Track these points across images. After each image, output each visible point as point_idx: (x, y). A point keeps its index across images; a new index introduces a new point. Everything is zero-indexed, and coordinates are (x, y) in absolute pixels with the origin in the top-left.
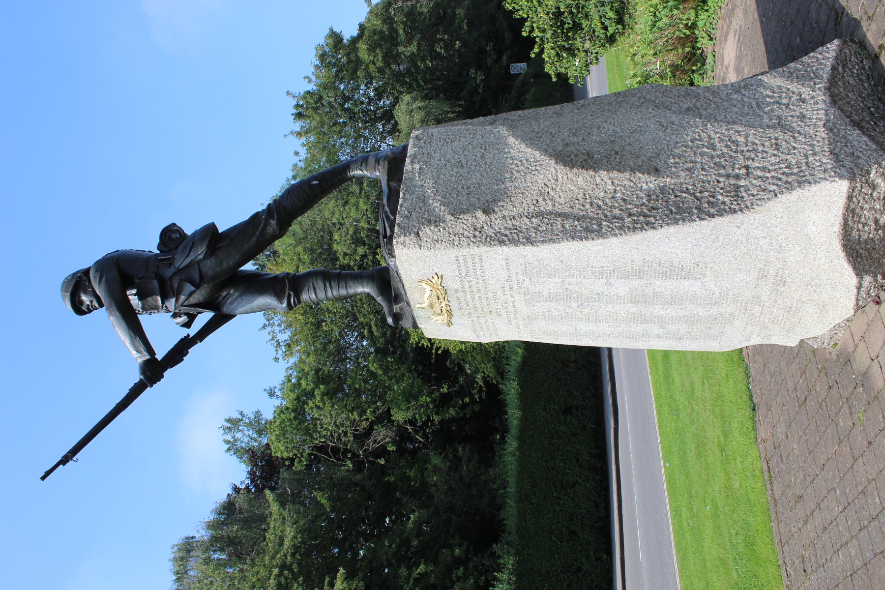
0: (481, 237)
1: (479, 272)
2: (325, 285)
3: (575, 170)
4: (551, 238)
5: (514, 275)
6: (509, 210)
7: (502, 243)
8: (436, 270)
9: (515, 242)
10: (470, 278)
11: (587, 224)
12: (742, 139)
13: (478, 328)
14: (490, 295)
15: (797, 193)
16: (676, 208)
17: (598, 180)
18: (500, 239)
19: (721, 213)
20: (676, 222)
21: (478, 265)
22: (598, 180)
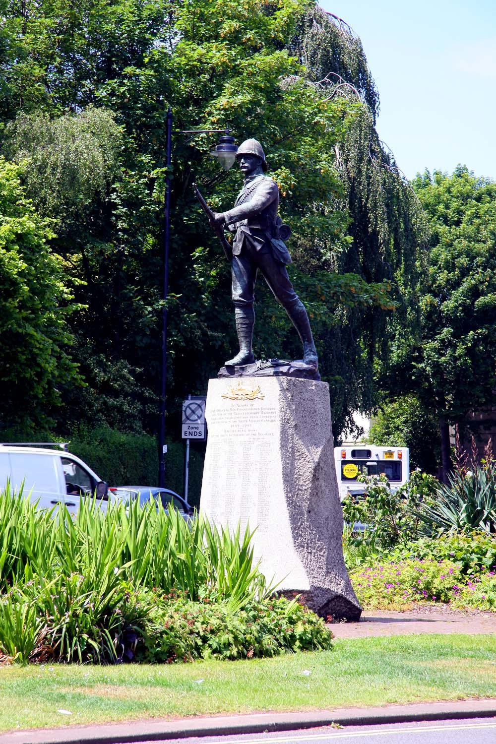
0: (285, 422)
1: (265, 419)
2: (244, 324)
3: (313, 471)
4: (284, 457)
5: (262, 437)
6: (296, 437)
7: (282, 433)
8: (266, 397)
9: (282, 439)
10: (260, 414)
11: (289, 477)
12: (322, 554)
13: (220, 413)
14: (248, 423)
15: (304, 570)
16: (294, 519)
17: (307, 482)
18: (284, 432)
19: (294, 537)
20: (290, 517)
21: (252, 411)
22: (307, 482)
